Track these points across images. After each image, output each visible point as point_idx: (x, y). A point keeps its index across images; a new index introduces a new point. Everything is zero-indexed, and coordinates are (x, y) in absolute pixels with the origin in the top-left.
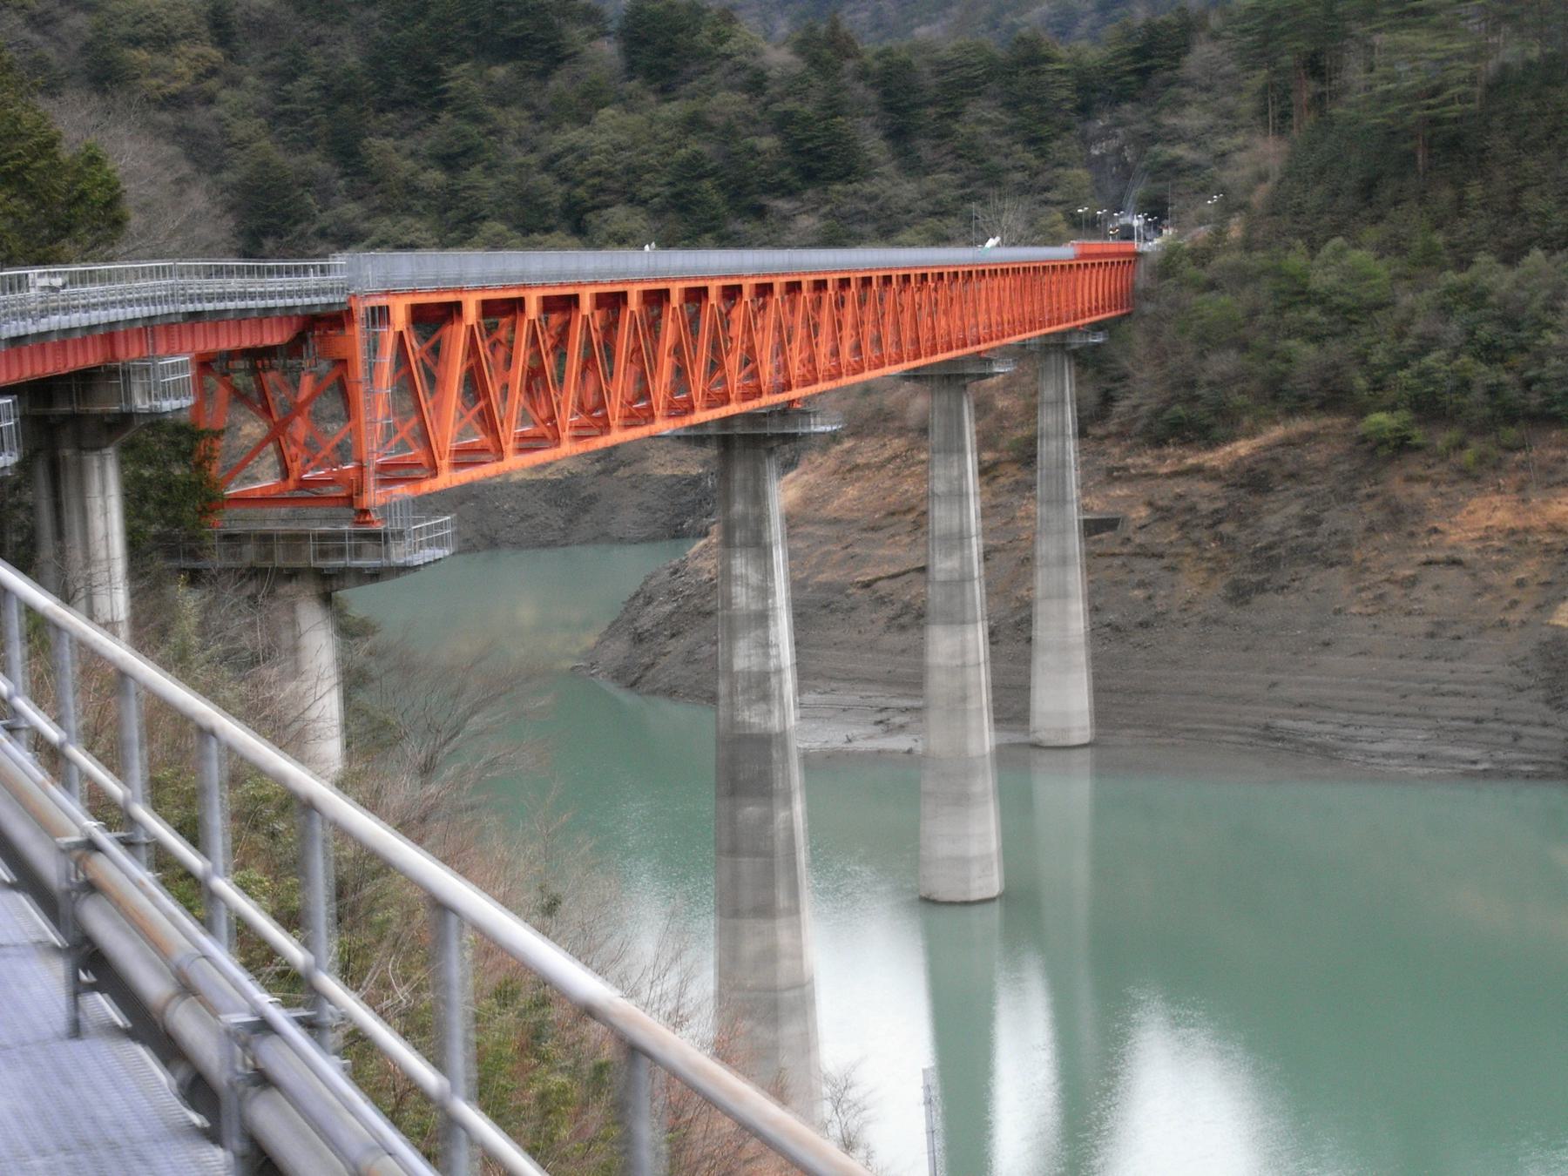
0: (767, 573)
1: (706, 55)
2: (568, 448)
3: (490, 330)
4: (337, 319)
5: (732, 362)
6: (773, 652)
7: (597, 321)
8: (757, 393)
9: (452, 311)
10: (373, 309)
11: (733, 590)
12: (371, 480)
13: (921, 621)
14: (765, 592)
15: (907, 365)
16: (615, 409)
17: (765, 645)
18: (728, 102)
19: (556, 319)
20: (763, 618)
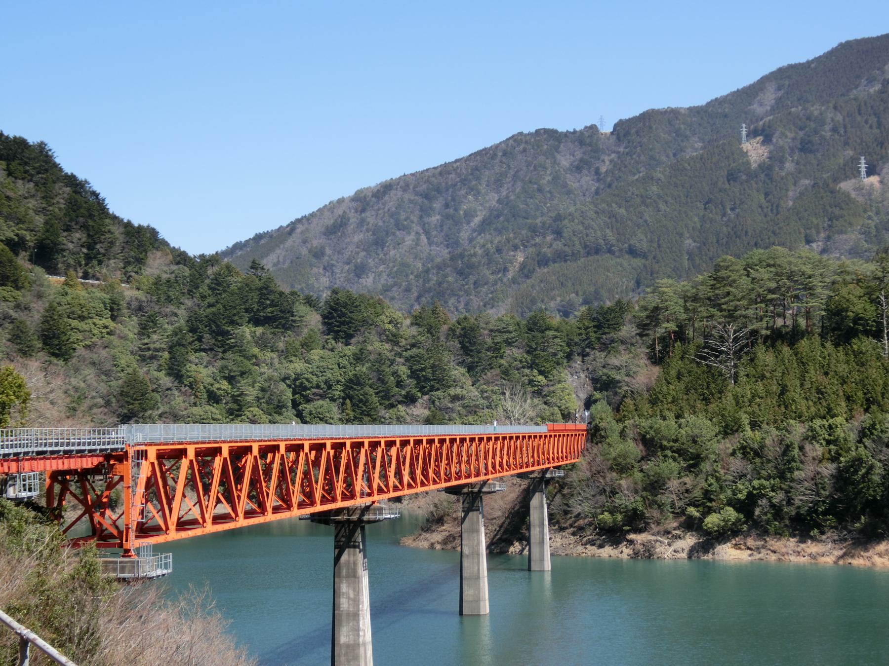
0: (357, 592)
1: (365, 322)
2: (296, 512)
3: (161, 465)
4: (122, 457)
5: (391, 472)
6: (361, 633)
7: (332, 453)
8: (352, 496)
9: (361, 444)
10: (138, 451)
11: (342, 600)
12: (132, 535)
13: (860, 307)
14: (356, 601)
15: (444, 485)
16: (318, 496)
17: (357, 630)
18: (376, 345)
19: (292, 455)
20: (356, 616)
